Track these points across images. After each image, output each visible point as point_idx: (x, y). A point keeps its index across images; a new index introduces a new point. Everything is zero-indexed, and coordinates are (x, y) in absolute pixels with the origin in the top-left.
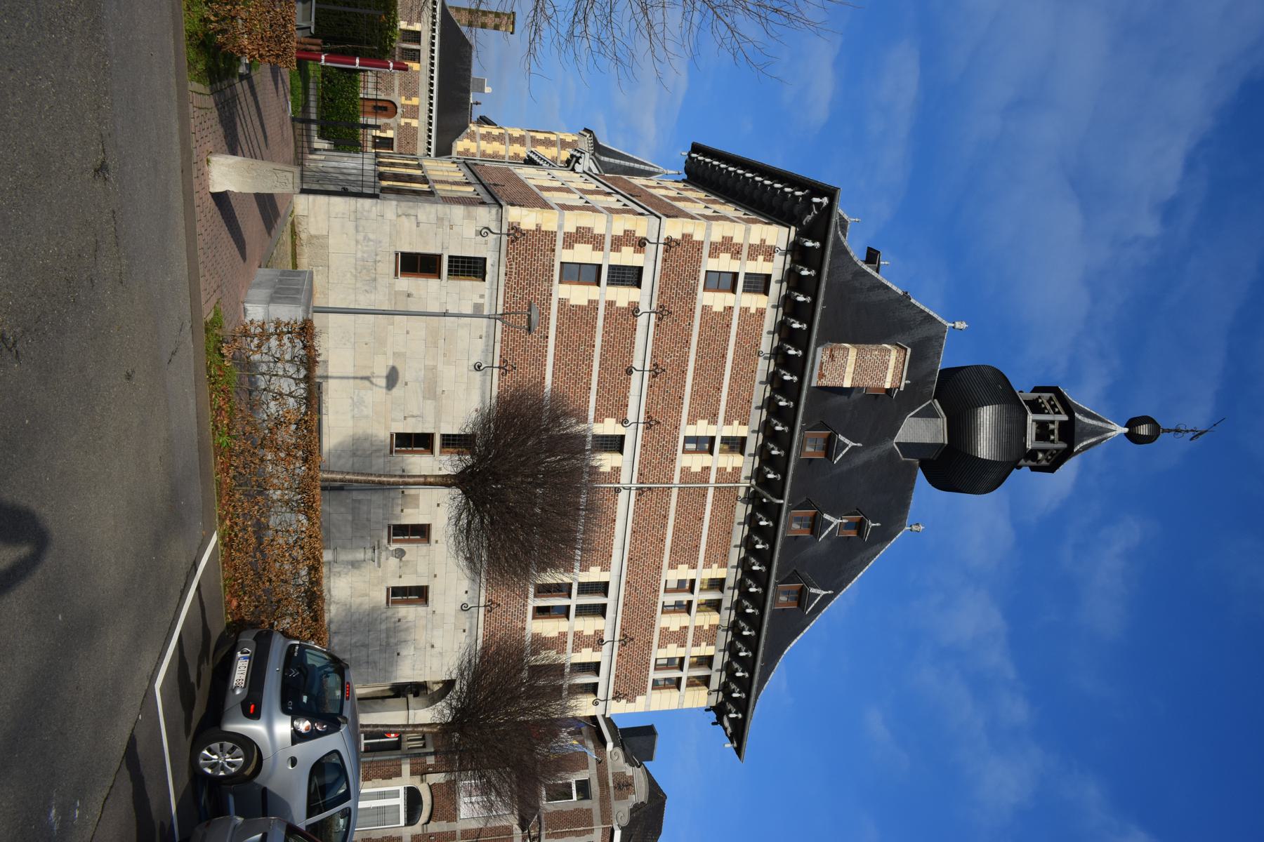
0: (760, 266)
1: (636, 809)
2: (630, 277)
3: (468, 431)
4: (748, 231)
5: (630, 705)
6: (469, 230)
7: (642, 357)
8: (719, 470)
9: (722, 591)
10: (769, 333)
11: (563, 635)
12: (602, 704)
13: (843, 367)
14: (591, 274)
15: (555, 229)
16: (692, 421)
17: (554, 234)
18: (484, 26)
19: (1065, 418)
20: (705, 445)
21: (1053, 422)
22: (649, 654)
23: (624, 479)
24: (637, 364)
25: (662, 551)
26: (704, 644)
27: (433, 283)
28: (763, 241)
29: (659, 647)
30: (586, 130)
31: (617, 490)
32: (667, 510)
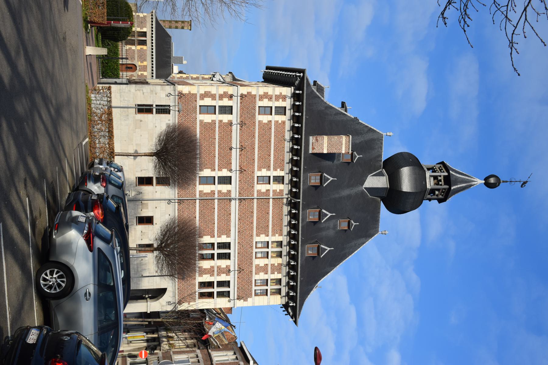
0: (281, 103)
2: (227, 110)
3: (159, 148)
5: (245, 302)
6: (163, 95)
7: (235, 143)
8: (273, 191)
9: (281, 247)
10: (288, 131)
11: (212, 267)
12: (232, 302)
13: (323, 144)
14: (211, 110)
15: (196, 93)
16: (260, 169)
17: (196, 94)
18: (177, 28)
19: (446, 174)
20: (268, 180)
21: (440, 176)
22: (252, 277)
23: (233, 196)
24: (234, 145)
25: (252, 228)
26: (276, 273)
27: (149, 116)
28: (281, 93)
29: (256, 274)
30: (230, 73)
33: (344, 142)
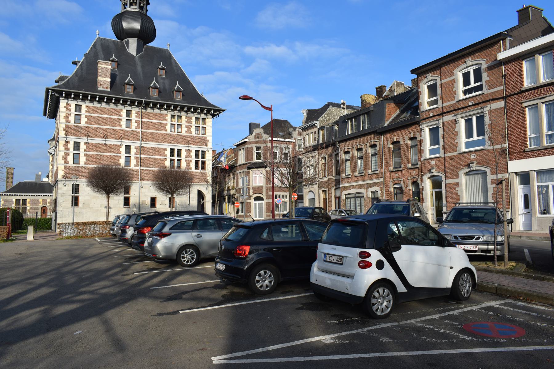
0: (73, 108)
1: (265, 133)
4: (62, 112)
6: (65, 188)
11: (186, 161)
13: (104, 81)
16: (121, 126)
18: (12, 178)
20: (128, 121)
23: (139, 145)
24: (103, 142)
25: (161, 134)
27: (80, 198)
28: (65, 107)
31: (141, 147)
32: (148, 132)
33: (103, 66)
